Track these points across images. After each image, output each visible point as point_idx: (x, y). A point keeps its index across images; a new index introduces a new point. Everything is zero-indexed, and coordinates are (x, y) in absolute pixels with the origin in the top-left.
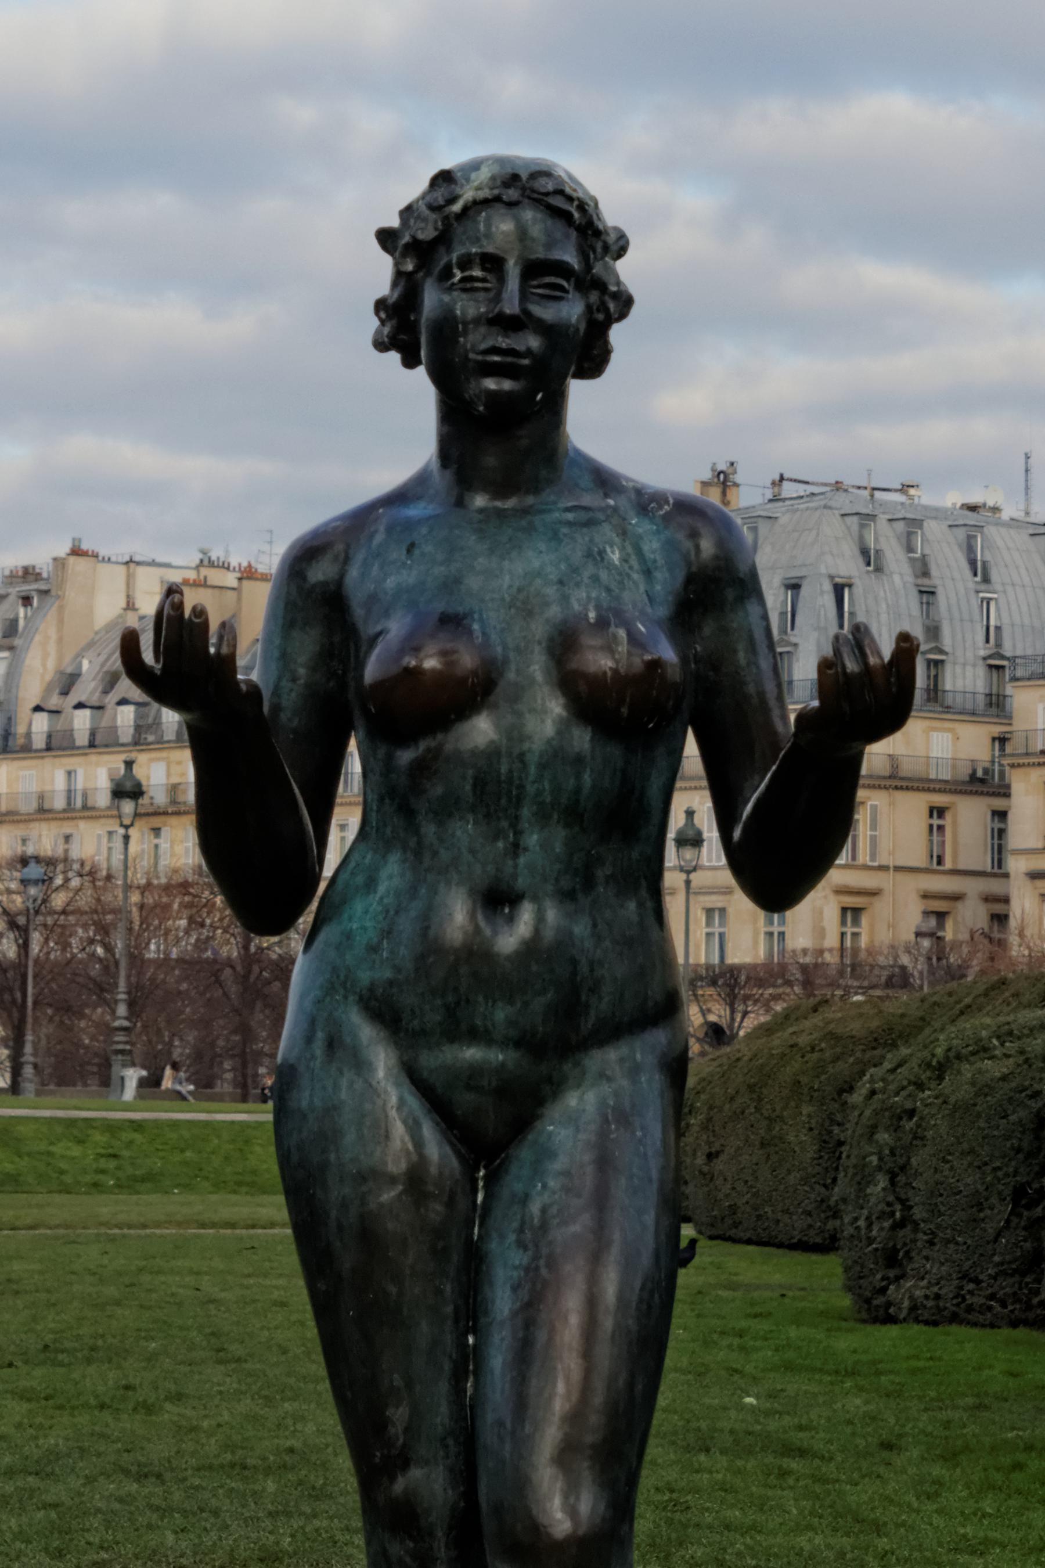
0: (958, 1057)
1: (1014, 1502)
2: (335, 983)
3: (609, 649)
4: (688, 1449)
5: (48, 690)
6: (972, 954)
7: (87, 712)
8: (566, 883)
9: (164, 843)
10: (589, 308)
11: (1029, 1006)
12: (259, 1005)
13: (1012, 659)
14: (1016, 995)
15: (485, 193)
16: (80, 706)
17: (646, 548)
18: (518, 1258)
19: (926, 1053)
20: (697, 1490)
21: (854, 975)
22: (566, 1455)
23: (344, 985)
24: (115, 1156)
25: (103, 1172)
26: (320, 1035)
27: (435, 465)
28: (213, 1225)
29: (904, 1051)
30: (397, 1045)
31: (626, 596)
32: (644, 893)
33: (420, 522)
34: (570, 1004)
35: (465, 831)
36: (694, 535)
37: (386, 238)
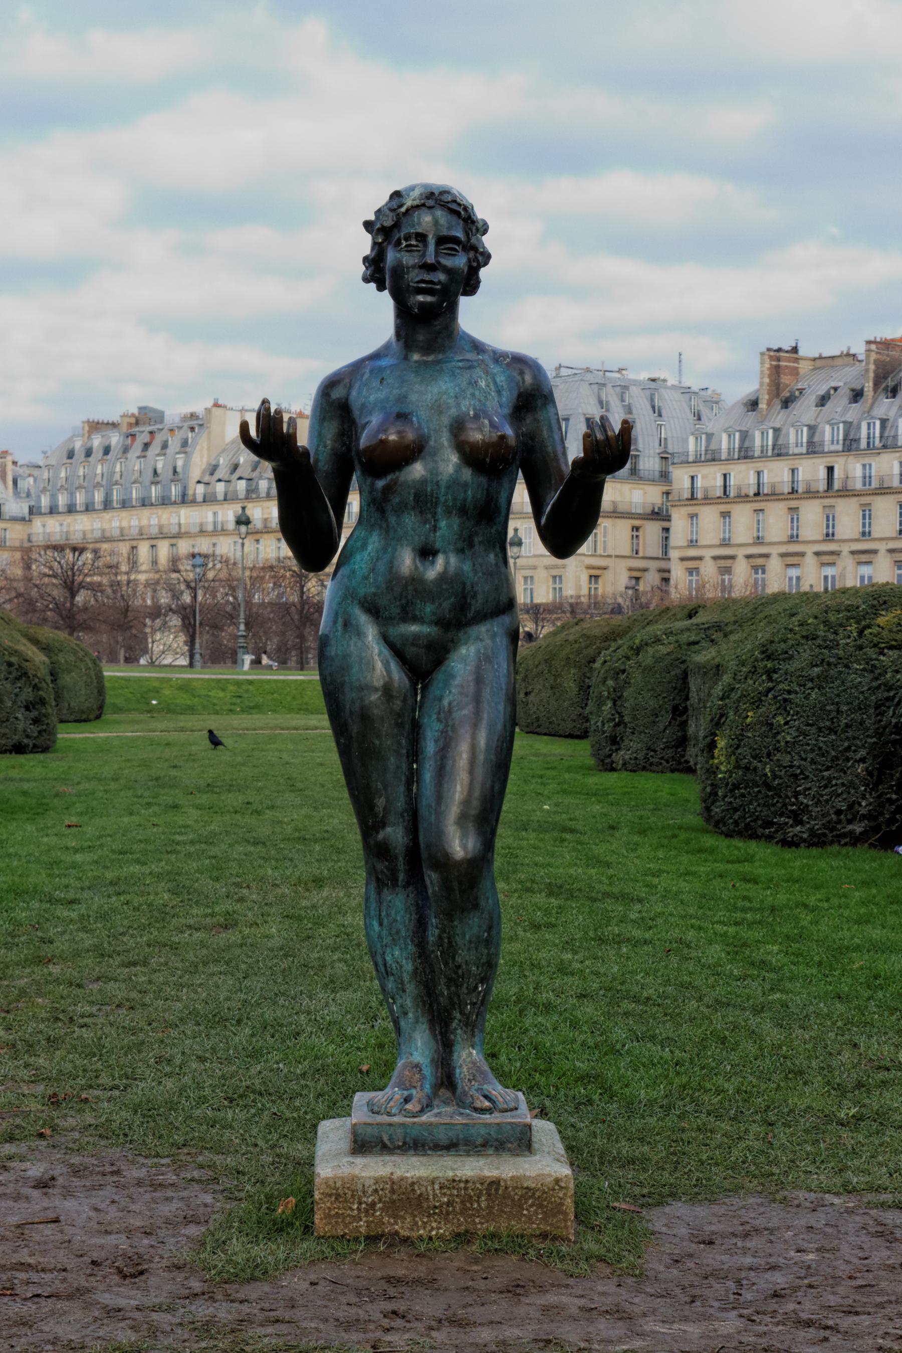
0: (646, 644)
2: (347, 595)
3: (480, 429)
4: (517, 829)
5: (203, 473)
7: (222, 484)
8: (460, 545)
9: (261, 547)
10: (469, 260)
11: (680, 619)
12: (308, 624)
13: (672, 454)
14: (674, 615)
15: (415, 203)
16: (219, 480)
17: (498, 380)
18: (437, 726)
19: (631, 643)
20: (522, 848)
21: (595, 608)
22: (462, 819)
26: (340, 620)
27: (394, 339)
28: (288, 729)
29: (620, 642)
30: (378, 624)
31: (488, 404)
32: (498, 550)
34: (462, 605)
35: (410, 520)
36: (522, 373)
37: (368, 225)
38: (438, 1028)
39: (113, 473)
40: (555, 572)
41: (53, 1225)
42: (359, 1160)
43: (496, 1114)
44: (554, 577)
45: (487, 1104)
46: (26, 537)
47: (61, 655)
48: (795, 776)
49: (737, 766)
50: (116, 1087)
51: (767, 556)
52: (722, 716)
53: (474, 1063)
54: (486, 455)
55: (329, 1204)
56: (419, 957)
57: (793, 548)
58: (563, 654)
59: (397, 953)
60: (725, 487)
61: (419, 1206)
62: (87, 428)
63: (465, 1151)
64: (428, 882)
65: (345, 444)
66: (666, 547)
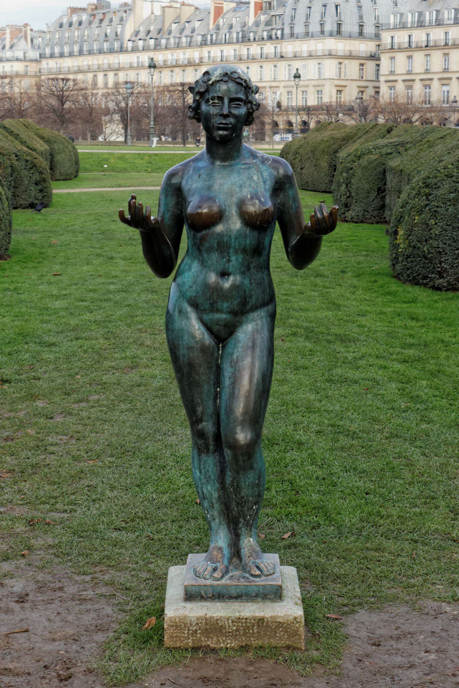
0: (364, 154)
1: (374, 295)
3: (254, 205)
5: (132, 35)
6: (370, 102)
8: (242, 270)
9: (162, 75)
10: (248, 109)
13: (382, 24)
15: (218, 79)
16: (140, 39)
23: (183, 296)
24: (151, 163)
25: (148, 167)
30: (197, 313)
33: (202, 168)
35: (215, 256)
38: (232, 526)
39: (84, 36)
40: (318, 89)
41: (24, 634)
42: (189, 605)
43: (263, 578)
44: (318, 91)
45: (258, 572)
46: (38, 70)
47: (55, 144)
48: (440, 252)
49: (409, 246)
50: (66, 511)
51: (431, 79)
52: (401, 217)
53: (251, 546)
54: (257, 220)
55: (172, 631)
56: (221, 490)
57: (445, 75)
58: (322, 147)
59: (209, 488)
60: (410, 42)
61: (221, 631)
62: (69, 11)
63: (246, 599)
64: (226, 454)
65: (179, 209)
66: (378, 75)
